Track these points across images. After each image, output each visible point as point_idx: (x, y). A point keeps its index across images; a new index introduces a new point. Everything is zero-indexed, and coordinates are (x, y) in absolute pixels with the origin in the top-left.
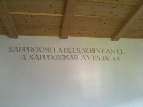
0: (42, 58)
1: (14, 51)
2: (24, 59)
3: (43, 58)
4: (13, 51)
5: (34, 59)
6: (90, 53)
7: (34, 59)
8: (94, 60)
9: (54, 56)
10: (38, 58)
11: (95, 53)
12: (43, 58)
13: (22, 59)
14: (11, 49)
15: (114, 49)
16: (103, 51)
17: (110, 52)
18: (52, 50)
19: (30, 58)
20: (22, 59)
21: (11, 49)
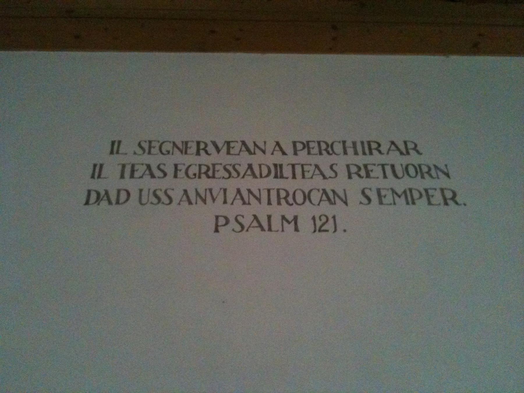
0: (301, 150)
1: (247, 230)
2: (187, 203)
3: (304, 148)
4: (246, 229)
5: (242, 174)
6: (318, 155)
7: (242, 174)
8: (163, 154)
9: (403, 176)
10: (260, 226)
11: (183, 142)
12: (304, 148)
13: (182, 203)
14: (240, 224)
15: (269, 217)
16: (306, 174)
17: (193, 201)
18: (154, 147)
19: (138, 148)
20: (182, 203)
21: (240, 224)
